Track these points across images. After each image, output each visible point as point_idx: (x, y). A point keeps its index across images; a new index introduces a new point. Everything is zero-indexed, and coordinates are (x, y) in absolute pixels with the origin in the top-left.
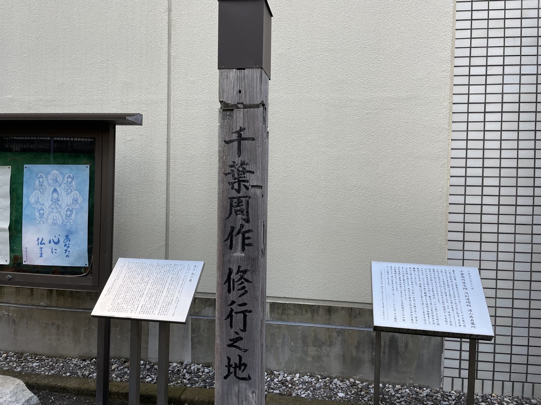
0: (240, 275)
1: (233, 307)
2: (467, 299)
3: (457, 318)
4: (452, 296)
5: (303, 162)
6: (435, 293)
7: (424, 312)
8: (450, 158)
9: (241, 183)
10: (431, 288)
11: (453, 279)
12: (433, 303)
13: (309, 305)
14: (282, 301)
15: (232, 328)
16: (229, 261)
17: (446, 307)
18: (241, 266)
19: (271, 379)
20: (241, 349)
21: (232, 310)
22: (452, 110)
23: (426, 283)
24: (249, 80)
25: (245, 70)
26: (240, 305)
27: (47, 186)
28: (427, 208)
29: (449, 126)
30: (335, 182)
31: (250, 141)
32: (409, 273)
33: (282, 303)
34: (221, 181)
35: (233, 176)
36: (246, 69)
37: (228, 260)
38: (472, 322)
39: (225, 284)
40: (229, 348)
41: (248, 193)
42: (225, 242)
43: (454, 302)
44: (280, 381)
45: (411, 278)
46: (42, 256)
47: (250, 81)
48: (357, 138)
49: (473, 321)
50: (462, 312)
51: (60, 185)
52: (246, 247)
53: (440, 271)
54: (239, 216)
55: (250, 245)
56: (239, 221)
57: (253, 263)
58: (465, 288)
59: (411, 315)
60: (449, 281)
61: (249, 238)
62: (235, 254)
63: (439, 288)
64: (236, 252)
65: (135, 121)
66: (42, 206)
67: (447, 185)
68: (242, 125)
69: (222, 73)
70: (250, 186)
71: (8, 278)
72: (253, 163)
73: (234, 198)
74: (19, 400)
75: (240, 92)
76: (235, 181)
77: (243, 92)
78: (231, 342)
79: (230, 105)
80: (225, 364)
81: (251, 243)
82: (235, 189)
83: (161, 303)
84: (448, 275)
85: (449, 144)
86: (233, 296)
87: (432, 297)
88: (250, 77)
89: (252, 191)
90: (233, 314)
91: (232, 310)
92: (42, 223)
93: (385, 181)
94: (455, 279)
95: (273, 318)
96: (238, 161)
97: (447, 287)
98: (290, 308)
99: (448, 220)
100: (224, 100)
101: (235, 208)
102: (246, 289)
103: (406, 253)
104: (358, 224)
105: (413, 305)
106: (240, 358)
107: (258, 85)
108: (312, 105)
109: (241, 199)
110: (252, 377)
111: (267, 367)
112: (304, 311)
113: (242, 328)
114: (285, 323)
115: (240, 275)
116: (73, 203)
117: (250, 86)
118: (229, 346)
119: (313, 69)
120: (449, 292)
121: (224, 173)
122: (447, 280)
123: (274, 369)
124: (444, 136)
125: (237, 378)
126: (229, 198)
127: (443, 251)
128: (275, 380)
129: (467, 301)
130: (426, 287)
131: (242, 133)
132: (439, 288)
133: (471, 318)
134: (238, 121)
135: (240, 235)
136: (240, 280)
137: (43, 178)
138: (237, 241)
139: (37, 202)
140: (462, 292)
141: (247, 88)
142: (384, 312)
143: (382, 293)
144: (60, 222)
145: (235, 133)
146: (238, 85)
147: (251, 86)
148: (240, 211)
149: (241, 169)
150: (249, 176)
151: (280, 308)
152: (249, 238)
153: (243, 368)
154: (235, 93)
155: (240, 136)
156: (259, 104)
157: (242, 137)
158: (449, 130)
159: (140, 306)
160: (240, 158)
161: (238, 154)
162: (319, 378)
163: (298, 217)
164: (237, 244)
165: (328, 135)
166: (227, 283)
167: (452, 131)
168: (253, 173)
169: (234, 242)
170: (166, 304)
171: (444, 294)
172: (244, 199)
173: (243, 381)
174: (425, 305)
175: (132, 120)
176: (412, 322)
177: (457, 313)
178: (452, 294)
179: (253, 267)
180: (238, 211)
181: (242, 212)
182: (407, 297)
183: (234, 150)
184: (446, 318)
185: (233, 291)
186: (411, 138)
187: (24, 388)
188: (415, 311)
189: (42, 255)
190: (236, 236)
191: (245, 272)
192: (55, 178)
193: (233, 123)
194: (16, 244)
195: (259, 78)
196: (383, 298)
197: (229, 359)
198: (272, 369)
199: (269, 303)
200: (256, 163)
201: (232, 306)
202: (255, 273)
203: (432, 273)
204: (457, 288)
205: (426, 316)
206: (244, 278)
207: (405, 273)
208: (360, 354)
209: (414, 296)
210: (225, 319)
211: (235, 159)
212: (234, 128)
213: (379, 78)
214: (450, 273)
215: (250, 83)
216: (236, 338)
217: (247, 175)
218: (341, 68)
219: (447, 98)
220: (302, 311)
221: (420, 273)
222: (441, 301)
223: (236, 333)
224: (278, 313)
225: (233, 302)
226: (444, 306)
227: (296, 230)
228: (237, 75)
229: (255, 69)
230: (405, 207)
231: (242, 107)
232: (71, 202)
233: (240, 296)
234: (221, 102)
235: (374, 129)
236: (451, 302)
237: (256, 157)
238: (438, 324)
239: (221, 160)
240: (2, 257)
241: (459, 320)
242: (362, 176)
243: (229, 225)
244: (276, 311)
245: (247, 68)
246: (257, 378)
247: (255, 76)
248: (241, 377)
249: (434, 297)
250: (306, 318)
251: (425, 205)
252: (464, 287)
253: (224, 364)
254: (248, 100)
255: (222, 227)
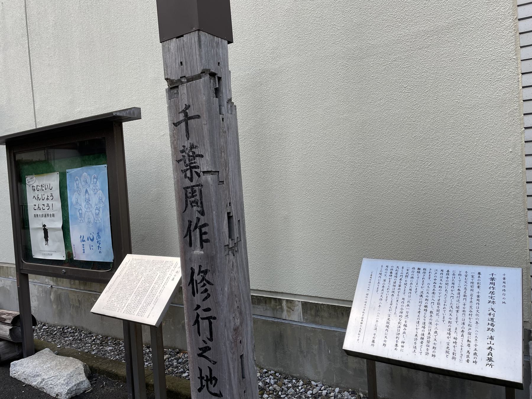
0: (202, 276)
1: (199, 311)
2: (490, 319)
3: (466, 348)
4: (467, 313)
5: (322, 135)
6: (441, 307)
7: (416, 335)
8: (522, 101)
9: (193, 170)
10: (436, 298)
11: (476, 285)
12: (434, 323)
13: (344, 307)
14: (315, 300)
15: (200, 336)
16: (190, 260)
17: (453, 330)
18: (202, 266)
19: (305, 390)
20: (210, 361)
21: (198, 316)
22: (518, 30)
23: (431, 291)
24: (188, 48)
25: (183, 36)
26: (205, 310)
27: (82, 188)
28: (493, 178)
29: (516, 55)
30: (362, 154)
31: (196, 119)
32: (410, 276)
33: (315, 303)
34: (175, 169)
35: (184, 162)
36: (184, 36)
37: (190, 259)
38: (490, 356)
39: (189, 285)
40: (199, 358)
41: (200, 181)
42: (185, 238)
43: (467, 323)
44: (314, 394)
45: (411, 284)
46: (84, 252)
47: (189, 48)
48: (385, 94)
49: (491, 355)
50: (476, 340)
51: (89, 186)
52: (204, 244)
53: (457, 273)
54: (195, 208)
55: (207, 241)
56: (195, 214)
57: (212, 263)
58: (492, 300)
59: (397, 337)
60: (469, 288)
61: (205, 233)
62: (195, 252)
63: (449, 299)
64: (196, 249)
65: (128, 116)
66: (80, 207)
67: (522, 142)
68: (187, 102)
69: (164, 46)
70: (201, 172)
71: (63, 272)
72: (201, 144)
73: (188, 188)
74: (70, 383)
75: (181, 63)
76: (187, 168)
77: (184, 63)
78: (200, 352)
79: (175, 81)
80: (198, 375)
81: (208, 239)
82: (188, 177)
83: (143, 303)
84: (469, 280)
85: (518, 81)
86: (198, 299)
87: (435, 312)
88: (189, 44)
89: (203, 177)
90: (200, 319)
91: (198, 316)
92: (82, 222)
93: (428, 145)
94: (478, 287)
95: (307, 319)
96: (187, 145)
97: (462, 297)
98: (324, 309)
99: (526, 193)
100: (169, 77)
101: (190, 200)
102: (209, 292)
103: (466, 242)
104: (395, 206)
105: (403, 322)
106: (211, 370)
107: (197, 51)
108: (326, 63)
109: (194, 189)
110: (223, 394)
111: (305, 376)
112: (340, 315)
113: (209, 337)
114: (320, 327)
115: (202, 276)
116: (99, 202)
117: (190, 54)
118: (200, 355)
119: (324, 18)
120: (464, 306)
121: (177, 161)
122: (465, 288)
123: (312, 378)
124: (511, 70)
125: (209, 392)
126: (184, 188)
127: (523, 239)
128: (308, 393)
129: (490, 322)
130: (430, 298)
131: (187, 111)
132: (449, 299)
133: (489, 351)
134: (183, 98)
135: (198, 230)
136: (202, 282)
137: (78, 180)
138: (196, 237)
139: (77, 203)
140: (485, 307)
141: (187, 57)
142: (360, 331)
143: (365, 303)
144: (92, 220)
145: (181, 112)
146: (179, 56)
147: (191, 54)
148: (195, 202)
149: (191, 154)
150: (199, 161)
151: (313, 309)
152: (205, 233)
153: (214, 382)
154: (177, 66)
155: (186, 115)
156: (200, 74)
157: (188, 116)
158: (517, 59)
159: (126, 305)
160: (189, 141)
161: (187, 136)
162: (361, 397)
163: (323, 201)
164: (196, 241)
165: (348, 97)
166: (191, 285)
167: (521, 60)
168: (202, 156)
169: (193, 238)
170: (146, 304)
171: (455, 309)
172: (196, 188)
173: (216, 397)
174: (421, 325)
175: (123, 114)
176: (395, 349)
177: (468, 341)
178: (467, 309)
179: (212, 267)
180: (193, 202)
181: (197, 203)
182: (399, 310)
183: (182, 133)
184: (448, 348)
185: (197, 294)
186: (459, 82)
187: (81, 372)
188: (404, 333)
189: (84, 251)
190: (194, 231)
191: (206, 272)
192: (85, 180)
193: (178, 101)
194: (68, 242)
195: (197, 43)
196: (364, 310)
197: (201, 370)
198: (311, 378)
199: (300, 302)
200: (204, 145)
201: (198, 311)
202: (215, 274)
203: (445, 276)
204: (478, 300)
205: (419, 340)
206: (205, 279)
207: (404, 275)
208: (411, 373)
209: (408, 310)
210: (193, 325)
211: (184, 142)
212: (180, 107)
213: (407, 8)
214: (473, 277)
215: (190, 51)
216: (204, 347)
217: (197, 159)
218: (357, 9)
219: (509, 13)
220: (337, 314)
221: (427, 274)
222: (447, 320)
223: (204, 341)
224: (311, 314)
225: (198, 307)
226: (423, 332)
227: (322, 217)
228: (177, 45)
229: (192, 33)
230: (458, 180)
231: (186, 81)
232: (98, 201)
233: (204, 300)
234: (167, 79)
235: (407, 79)
236: (463, 322)
237: (203, 137)
238: (433, 356)
239: (173, 146)
240: (61, 253)
241: (468, 351)
242: (396, 143)
243: (187, 219)
244: (309, 312)
245: (185, 34)
246: (228, 396)
247: (193, 41)
248: (213, 392)
249: (438, 312)
250: (343, 322)
251: (489, 174)
252: (490, 299)
253: (197, 375)
254: (189, 72)
255: (181, 222)
